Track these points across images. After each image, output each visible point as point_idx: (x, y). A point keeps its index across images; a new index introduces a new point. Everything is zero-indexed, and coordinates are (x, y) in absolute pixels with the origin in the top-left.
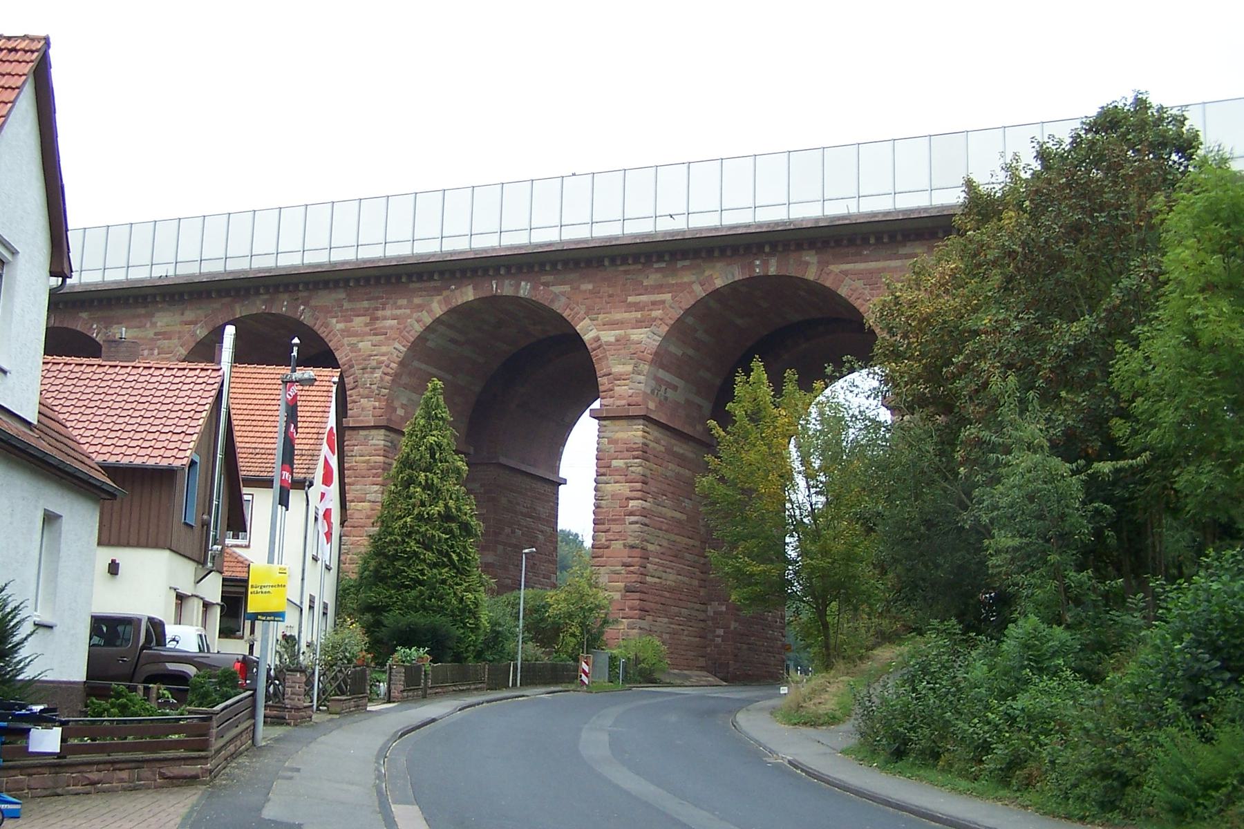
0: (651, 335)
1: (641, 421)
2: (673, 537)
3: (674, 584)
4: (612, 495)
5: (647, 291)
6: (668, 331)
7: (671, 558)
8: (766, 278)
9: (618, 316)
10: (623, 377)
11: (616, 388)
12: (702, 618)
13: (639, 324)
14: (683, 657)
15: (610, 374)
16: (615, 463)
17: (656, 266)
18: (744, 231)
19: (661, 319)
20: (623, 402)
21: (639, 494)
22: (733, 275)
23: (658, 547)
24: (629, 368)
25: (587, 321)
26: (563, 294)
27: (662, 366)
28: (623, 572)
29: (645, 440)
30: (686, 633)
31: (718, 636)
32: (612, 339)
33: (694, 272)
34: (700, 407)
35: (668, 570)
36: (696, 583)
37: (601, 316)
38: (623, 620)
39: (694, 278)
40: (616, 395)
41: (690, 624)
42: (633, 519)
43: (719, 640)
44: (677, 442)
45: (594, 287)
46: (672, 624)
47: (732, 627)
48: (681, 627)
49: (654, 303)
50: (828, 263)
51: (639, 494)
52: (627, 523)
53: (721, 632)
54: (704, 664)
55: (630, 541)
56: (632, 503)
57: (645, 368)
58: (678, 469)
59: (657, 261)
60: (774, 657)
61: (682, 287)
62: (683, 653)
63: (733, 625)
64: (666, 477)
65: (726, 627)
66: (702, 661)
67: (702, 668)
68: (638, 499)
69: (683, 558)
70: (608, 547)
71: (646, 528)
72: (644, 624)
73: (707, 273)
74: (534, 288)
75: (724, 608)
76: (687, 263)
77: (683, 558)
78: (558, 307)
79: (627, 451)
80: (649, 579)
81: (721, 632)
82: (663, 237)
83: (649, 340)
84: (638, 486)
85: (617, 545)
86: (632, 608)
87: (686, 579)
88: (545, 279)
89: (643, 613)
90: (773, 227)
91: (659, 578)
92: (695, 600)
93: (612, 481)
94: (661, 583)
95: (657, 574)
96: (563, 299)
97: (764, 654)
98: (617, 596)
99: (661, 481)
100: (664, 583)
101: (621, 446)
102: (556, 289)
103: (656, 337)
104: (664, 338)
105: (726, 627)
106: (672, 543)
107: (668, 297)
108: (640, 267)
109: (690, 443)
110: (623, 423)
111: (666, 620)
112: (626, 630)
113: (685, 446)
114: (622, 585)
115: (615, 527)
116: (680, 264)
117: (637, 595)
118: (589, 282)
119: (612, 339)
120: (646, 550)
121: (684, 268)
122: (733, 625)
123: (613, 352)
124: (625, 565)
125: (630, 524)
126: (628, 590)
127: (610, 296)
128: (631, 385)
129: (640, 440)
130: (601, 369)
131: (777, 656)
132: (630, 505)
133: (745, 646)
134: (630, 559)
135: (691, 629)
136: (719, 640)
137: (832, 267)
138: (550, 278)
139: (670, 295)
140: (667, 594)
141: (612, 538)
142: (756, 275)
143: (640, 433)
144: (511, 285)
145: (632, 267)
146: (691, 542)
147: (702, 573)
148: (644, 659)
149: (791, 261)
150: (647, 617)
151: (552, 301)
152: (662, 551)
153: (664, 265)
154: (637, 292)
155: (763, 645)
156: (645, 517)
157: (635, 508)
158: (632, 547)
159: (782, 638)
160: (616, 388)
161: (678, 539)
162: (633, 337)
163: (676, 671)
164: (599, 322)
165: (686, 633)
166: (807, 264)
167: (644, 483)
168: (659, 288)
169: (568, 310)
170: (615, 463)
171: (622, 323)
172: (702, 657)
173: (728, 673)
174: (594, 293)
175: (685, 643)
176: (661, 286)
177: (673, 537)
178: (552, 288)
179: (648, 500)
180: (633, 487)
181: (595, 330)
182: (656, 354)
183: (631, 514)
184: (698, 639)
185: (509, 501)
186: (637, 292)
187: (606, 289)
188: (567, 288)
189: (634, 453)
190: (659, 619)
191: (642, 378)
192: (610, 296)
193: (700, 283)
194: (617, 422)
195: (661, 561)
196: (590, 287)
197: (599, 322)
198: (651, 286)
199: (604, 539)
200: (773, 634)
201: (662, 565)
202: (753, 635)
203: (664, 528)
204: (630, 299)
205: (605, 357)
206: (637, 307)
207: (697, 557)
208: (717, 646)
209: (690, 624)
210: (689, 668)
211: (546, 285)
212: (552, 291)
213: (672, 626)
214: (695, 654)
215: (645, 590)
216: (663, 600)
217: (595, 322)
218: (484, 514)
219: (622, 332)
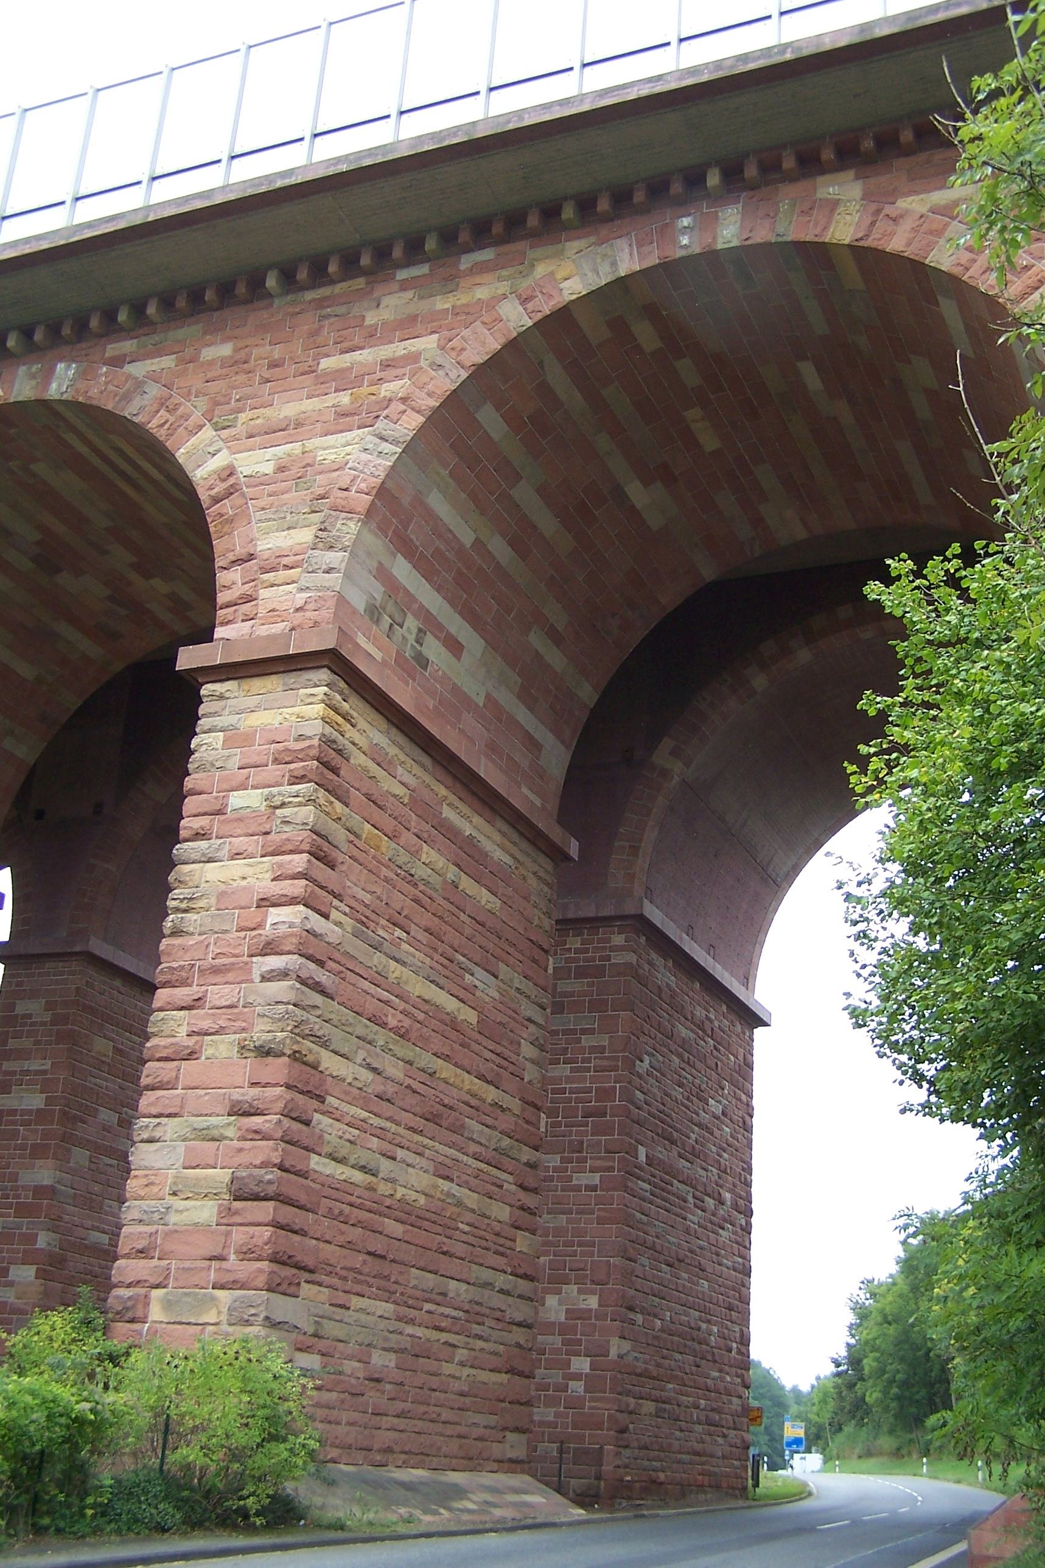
0: (371, 441)
1: (324, 675)
2: (426, 1060)
3: (422, 1200)
4: (222, 895)
5: (372, 337)
6: (422, 428)
7: (420, 1123)
8: (711, 257)
9: (288, 409)
10: (285, 561)
11: (263, 593)
12: (519, 1318)
13: (344, 419)
14: (450, 1430)
15: (251, 557)
16: (237, 800)
17: (402, 275)
18: (645, 91)
19: (404, 400)
20: (279, 628)
21: (298, 887)
22: (614, 264)
23: (366, 1076)
24: (305, 536)
25: (208, 432)
26: (154, 377)
27: (404, 546)
28: (230, 1132)
29: (328, 730)
30: (461, 1354)
31: (577, 1377)
32: (268, 468)
33: (504, 273)
34: (533, 745)
35: (400, 1153)
36: (502, 1212)
37: (243, 417)
38: (219, 1293)
39: (503, 287)
40: (262, 611)
41: (476, 1329)
42: (274, 962)
43: (577, 1387)
44: (452, 798)
45: (236, 350)
46: (411, 1321)
47: (613, 1353)
48: (444, 1337)
49: (387, 365)
50: (892, 196)
51: (298, 887)
52: (258, 979)
53: (582, 1364)
54: (520, 1453)
55: (261, 1033)
56: (276, 915)
57: (349, 529)
58: (452, 872)
59: (408, 264)
60: (724, 1436)
61: (466, 315)
62: (446, 1415)
63: (616, 1347)
64: (410, 879)
65: (598, 1353)
66: (515, 1446)
67: (513, 1465)
68: (293, 901)
69: (457, 1129)
70: (192, 1055)
71: (318, 999)
72: (284, 1308)
73: (541, 270)
74: (84, 375)
75: (593, 1302)
76: (487, 255)
77: (457, 1129)
78: (137, 409)
79: (276, 761)
80: (315, 1162)
81: (582, 1364)
82: (413, 148)
83: (365, 457)
84: (299, 862)
85: (221, 1048)
86: (247, 1254)
87: (471, 1199)
88: (113, 349)
89: (288, 1272)
90: (732, 67)
91: (363, 1169)
92: (500, 1261)
93: (224, 853)
94: (371, 1188)
95: (361, 1156)
96: (154, 390)
97: (698, 1428)
98: (206, 1212)
99: (387, 880)
100: (384, 1188)
101: (259, 751)
102: (137, 369)
103: (387, 447)
104: (409, 449)
105: (598, 1353)
106: (423, 1077)
107: (427, 344)
108: (360, 282)
109: (500, 824)
110: (272, 683)
111: (387, 1308)
112: (224, 1327)
113: (477, 819)
114: (223, 1175)
115: (220, 993)
116: (466, 261)
117: (266, 1210)
118: (225, 340)
119: (268, 468)
120: (315, 1066)
121: (472, 271)
122: (616, 1347)
123: (264, 501)
124: (240, 1110)
125: (264, 979)
126: (242, 1192)
127: (274, 365)
128: (306, 580)
129: (315, 728)
130: (224, 547)
131: (732, 1433)
132: (269, 921)
133: (649, 1407)
134: (255, 1091)
135: (480, 1344)
136: (577, 1387)
137: (903, 203)
138: (128, 346)
139: (435, 336)
140: (397, 1229)
141: (205, 1024)
142: (680, 253)
143: (319, 709)
144: (33, 376)
145: (338, 288)
146: (491, 1094)
147: (521, 1186)
148: (195, 1430)
149: (784, 206)
150: (306, 1289)
151: (127, 398)
152: (380, 1088)
153: (424, 269)
154: (345, 345)
155: (697, 1407)
156: (320, 963)
157: (283, 929)
158: (265, 1052)
159: (741, 1389)
160: (263, 593)
161: (446, 1070)
162: (321, 455)
163: (418, 1474)
164: (240, 429)
165: (461, 1354)
166: (833, 205)
167: (317, 855)
168: (408, 326)
169: (162, 412)
170: (237, 800)
171: (299, 424)
172: (518, 1430)
173: (598, 1478)
174: (238, 363)
175: (456, 1386)
176: (413, 319)
177: (426, 1060)
178: (130, 369)
179: (335, 915)
180: (280, 865)
181: (225, 451)
182: (383, 492)
183: (269, 948)
184: (504, 1378)
185: (117, 1050)
186: (345, 345)
187: (263, 350)
188: (167, 362)
189: (292, 766)
190: (356, 1302)
191: (336, 558)
192: (274, 365)
193: (519, 297)
194: (257, 684)
195: (375, 1121)
196: (226, 350)
197: (240, 429)
198: (385, 323)
199: (183, 1031)
200: (723, 1380)
201: (380, 1134)
202: (672, 1379)
203: (392, 1022)
204: (325, 364)
205: (243, 513)
206: (342, 380)
207: (506, 1142)
208: (574, 1404)
209: (476, 1329)
210: (471, 1462)
211: (118, 362)
212: (129, 376)
213: (410, 1330)
214: (493, 1420)
215: (303, 1199)
216: (377, 1244)
217: (225, 433)
218: (45, 1072)
219: (296, 448)
